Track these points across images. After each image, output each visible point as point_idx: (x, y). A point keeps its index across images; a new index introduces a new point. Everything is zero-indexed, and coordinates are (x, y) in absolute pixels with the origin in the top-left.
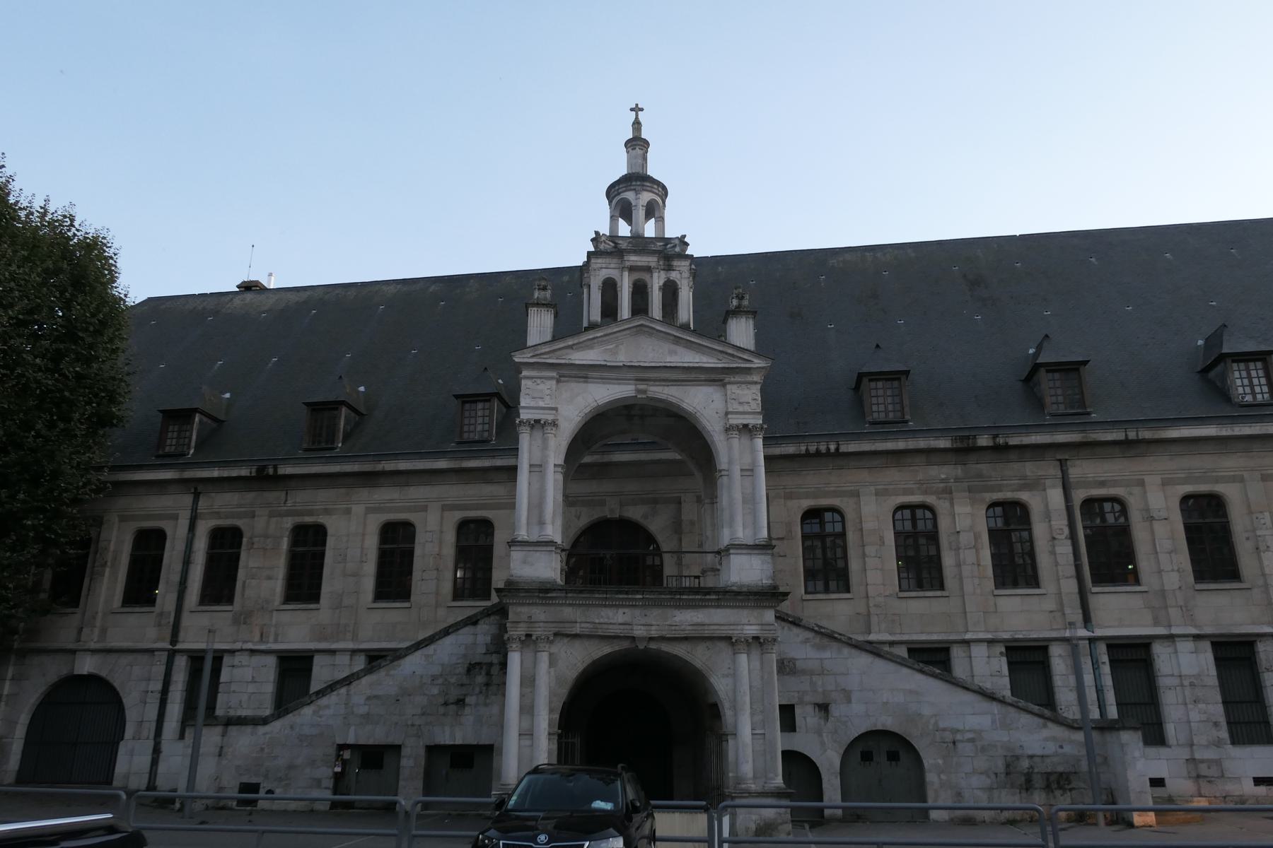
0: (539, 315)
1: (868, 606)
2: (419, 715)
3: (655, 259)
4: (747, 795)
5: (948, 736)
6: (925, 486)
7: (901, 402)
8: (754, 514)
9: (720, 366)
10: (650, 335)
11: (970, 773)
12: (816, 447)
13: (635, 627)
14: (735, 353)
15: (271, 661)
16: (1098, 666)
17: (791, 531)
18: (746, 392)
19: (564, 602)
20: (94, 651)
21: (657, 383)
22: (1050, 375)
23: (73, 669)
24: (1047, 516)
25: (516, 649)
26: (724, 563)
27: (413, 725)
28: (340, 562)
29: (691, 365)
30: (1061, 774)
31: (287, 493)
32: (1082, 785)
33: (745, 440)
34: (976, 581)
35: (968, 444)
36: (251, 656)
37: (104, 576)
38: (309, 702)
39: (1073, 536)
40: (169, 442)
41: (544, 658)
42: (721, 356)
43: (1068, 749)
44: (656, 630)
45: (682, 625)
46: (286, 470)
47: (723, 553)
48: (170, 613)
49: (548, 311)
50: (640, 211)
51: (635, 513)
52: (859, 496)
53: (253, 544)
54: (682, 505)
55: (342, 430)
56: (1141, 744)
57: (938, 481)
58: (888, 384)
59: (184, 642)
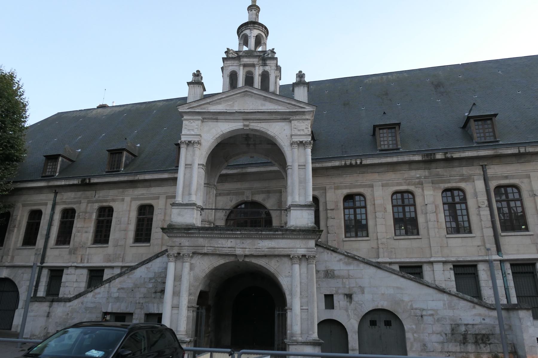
0: (194, 88)
1: (378, 244)
2: (142, 298)
3: (257, 60)
4: (296, 343)
5: (419, 313)
6: (408, 181)
7: (396, 140)
8: (305, 189)
9: (288, 110)
10: (252, 96)
11: (431, 333)
12: (350, 162)
13: (237, 249)
14: (296, 104)
15: (85, 272)
16: (506, 275)
17: (337, 206)
18: (302, 124)
19: (198, 235)
20: (8, 267)
21: (255, 121)
22: (476, 123)
24: (476, 195)
25: (172, 261)
26: (288, 215)
27: (139, 303)
28: (118, 224)
29: (272, 110)
30: (484, 335)
31: (96, 192)
32: (496, 341)
33: (301, 149)
34: (436, 230)
35: (431, 158)
36: (76, 269)
37: (13, 232)
38: (91, 291)
39: (490, 206)
40: (48, 170)
41: (187, 265)
42: (289, 106)
43: (488, 321)
44: (248, 251)
45: (263, 248)
46: (94, 180)
47: (288, 210)
48: (41, 249)
49: (198, 86)
50: (252, 39)
51: (259, 198)
52: (373, 187)
53: (80, 216)
54: (282, 194)
55: (124, 162)
56: (531, 318)
57: (416, 178)
58: (390, 131)
59: (47, 263)
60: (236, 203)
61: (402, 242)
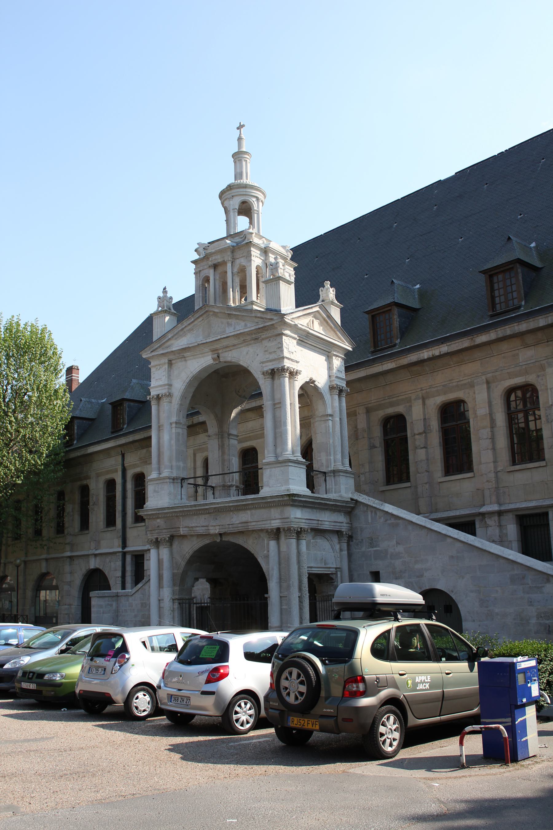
13: (210, 528)
23: (89, 566)
60: (307, 440)
61: (518, 475)
